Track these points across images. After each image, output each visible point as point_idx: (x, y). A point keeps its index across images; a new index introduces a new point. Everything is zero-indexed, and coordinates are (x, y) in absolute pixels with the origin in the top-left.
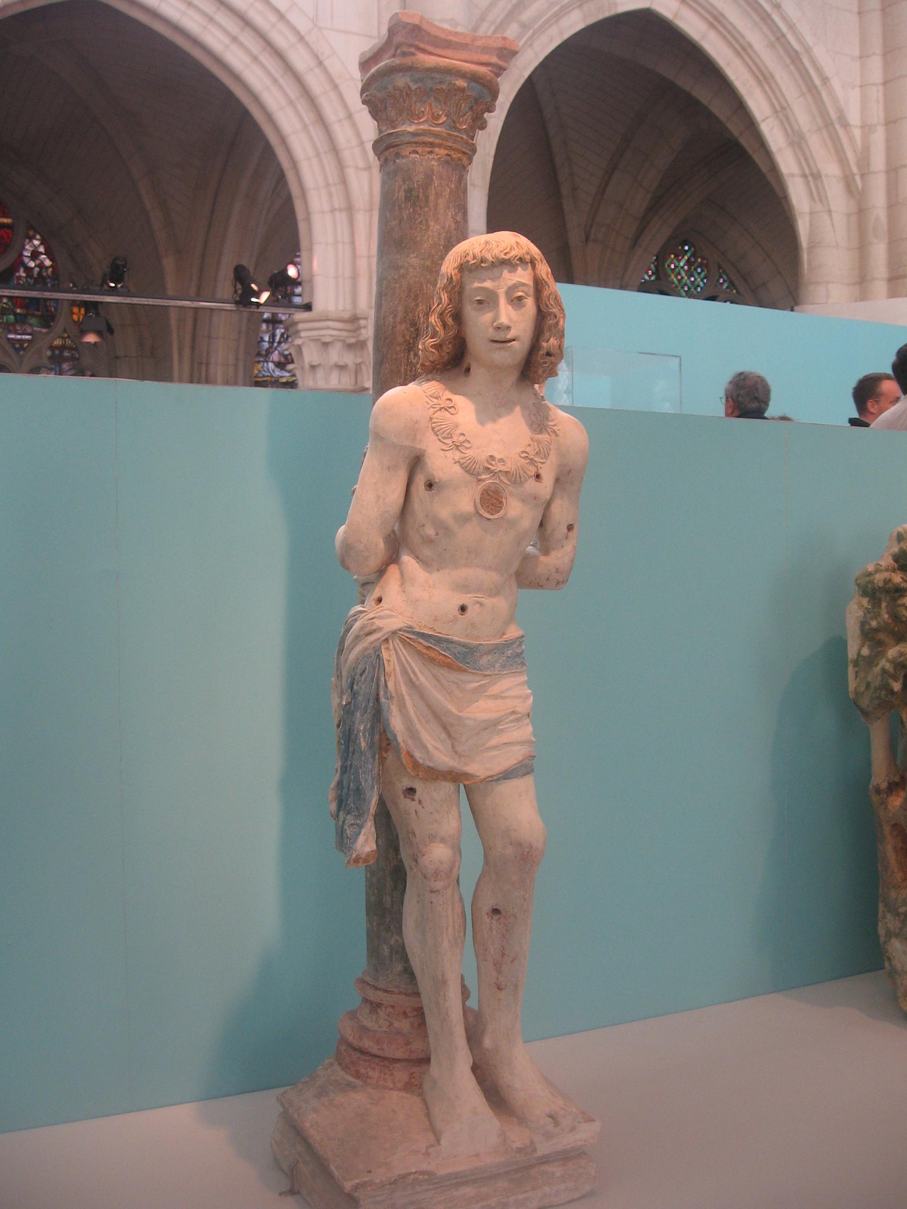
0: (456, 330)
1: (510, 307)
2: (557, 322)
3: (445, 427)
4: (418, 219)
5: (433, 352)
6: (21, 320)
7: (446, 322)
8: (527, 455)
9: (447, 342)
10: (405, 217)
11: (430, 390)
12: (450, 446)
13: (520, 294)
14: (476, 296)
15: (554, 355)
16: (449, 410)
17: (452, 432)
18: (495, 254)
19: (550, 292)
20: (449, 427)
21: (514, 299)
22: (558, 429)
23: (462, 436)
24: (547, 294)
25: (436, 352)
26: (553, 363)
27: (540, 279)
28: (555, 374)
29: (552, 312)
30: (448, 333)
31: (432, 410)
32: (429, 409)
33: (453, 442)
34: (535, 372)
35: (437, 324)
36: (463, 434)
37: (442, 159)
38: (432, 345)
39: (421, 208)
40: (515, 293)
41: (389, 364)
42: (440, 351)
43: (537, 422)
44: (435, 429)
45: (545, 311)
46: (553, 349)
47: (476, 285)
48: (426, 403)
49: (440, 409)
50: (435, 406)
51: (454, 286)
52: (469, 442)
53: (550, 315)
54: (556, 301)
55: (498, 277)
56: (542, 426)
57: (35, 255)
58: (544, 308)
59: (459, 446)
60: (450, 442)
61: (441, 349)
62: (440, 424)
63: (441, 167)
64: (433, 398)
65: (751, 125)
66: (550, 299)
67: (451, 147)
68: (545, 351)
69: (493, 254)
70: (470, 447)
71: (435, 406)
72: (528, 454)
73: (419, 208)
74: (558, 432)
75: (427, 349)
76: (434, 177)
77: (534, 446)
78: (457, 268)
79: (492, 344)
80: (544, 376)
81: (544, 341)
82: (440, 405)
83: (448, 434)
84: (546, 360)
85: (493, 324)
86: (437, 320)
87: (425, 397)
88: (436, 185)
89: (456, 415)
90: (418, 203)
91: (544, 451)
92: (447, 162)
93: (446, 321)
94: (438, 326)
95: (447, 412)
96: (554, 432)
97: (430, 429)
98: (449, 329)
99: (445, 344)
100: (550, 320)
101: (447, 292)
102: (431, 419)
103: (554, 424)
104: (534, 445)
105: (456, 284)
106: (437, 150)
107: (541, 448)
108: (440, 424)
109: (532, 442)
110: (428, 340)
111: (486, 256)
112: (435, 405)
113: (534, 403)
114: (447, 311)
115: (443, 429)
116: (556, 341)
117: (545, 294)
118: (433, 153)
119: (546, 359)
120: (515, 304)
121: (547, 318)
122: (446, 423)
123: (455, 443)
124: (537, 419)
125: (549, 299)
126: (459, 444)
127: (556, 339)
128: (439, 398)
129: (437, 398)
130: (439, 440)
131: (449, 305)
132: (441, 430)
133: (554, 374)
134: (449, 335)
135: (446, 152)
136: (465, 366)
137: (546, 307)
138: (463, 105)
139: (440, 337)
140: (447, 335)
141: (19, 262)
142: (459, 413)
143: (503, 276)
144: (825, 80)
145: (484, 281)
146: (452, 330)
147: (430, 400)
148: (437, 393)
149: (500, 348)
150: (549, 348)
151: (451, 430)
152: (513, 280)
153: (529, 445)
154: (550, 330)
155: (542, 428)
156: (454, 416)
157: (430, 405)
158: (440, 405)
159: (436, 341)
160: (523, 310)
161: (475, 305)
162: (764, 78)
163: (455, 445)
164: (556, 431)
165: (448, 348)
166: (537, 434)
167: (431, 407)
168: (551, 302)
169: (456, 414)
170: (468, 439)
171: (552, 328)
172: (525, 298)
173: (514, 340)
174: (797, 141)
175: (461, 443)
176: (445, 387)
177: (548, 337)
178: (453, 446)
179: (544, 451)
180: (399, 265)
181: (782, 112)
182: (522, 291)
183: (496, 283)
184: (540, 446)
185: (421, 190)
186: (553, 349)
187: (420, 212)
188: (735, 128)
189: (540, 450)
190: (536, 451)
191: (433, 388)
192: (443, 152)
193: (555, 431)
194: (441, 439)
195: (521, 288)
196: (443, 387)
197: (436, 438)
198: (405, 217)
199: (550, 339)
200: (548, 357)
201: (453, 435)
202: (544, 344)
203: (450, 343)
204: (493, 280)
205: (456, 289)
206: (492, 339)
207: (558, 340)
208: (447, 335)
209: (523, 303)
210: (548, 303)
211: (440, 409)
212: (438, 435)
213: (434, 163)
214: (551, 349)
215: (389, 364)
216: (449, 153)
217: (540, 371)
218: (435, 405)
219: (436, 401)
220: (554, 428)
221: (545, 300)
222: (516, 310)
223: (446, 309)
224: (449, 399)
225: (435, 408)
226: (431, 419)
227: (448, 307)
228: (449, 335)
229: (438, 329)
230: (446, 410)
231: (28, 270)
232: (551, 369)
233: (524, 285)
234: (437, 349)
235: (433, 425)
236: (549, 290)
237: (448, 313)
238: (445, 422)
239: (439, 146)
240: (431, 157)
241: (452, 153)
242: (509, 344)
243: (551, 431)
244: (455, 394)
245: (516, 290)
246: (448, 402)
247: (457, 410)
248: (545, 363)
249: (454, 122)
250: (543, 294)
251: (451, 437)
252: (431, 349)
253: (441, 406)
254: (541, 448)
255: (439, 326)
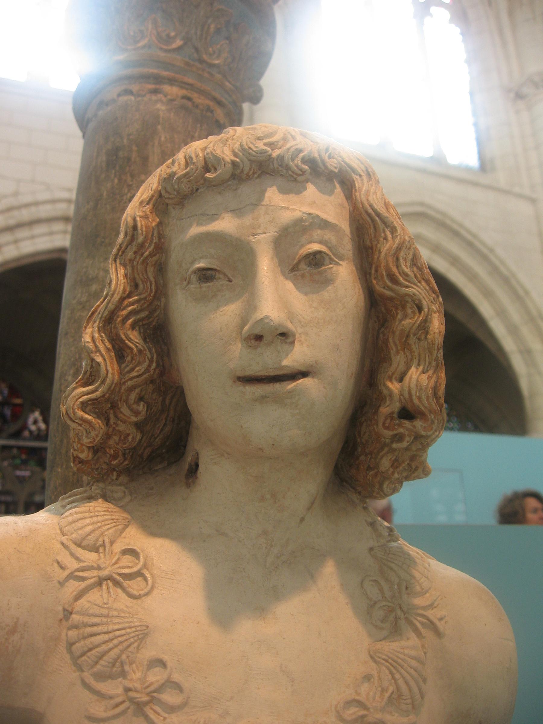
0: (151, 361)
1: (289, 285)
2: (425, 321)
3: (106, 642)
4: (126, 194)
5: (89, 423)
6: (25, 462)
7: (123, 341)
8: (363, 712)
9: (133, 396)
10: (105, 194)
11: (79, 524)
12: (117, 705)
13: (316, 247)
14: (193, 263)
15: (422, 415)
16: (125, 584)
17: (124, 657)
18: (241, 146)
19: (397, 241)
20: (116, 642)
21: (300, 261)
22: (439, 616)
23: (157, 669)
24: (391, 248)
25: (98, 423)
26: (422, 436)
27: (369, 215)
28: (424, 470)
29: (407, 295)
30: (132, 370)
31: (73, 587)
32: (61, 584)
33: (127, 690)
34: (369, 468)
35: (96, 346)
36: (162, 664)
37: (176, 103)
38: (82, 403)
39: (133, 176)
40: (302, 246)
41: (62, 467)
42: (112, 421)
43: (384, 603)
44: (74, 647)
45: (388, 293)
46: (419, 398)
47: (195, 230)
48: (56, 565)
49: (99, 583)
50: (84, 574)
51: (142, 246)
52: (178, 687)
53: (404, 307)
54: (415, 269)
55: (252, 204)
56: (399, 612)
57: (35, 422)
58: (385, 287)
59: (146, 703)
60: (120, 690)
61: (116, 416)
62: (89, 630)
63: (172, 114)
64: (84, 548)
65: (482, 323)
66: (401, 260)
67: (191, 85)
68: (396, 406)
69: (237, 146)
70: (184, 704)
71: (84, 574)
72: (366, 708)
73: (128, 175)
74: (440, 625)
75: (72, 415)
76: (159, 127)
77: (380, 679)
78: (148, 204)
79: (241, 388)
80: (396, 475)
81: (390, 379)
82: (99, 568)
83: (114, 665)
84: (401, 430)
85: (241, 332)
86: (96, 335)
87: (59, 546)
88: (163, 139)
89: (148, 601)
90: (127, 168)
91: (410, 690)
92: (183, 107)
93: (123, 337)
94: (98, 350)
95: (119, 591)
96: (432, 626)
97: (62, 648)
98: (132, 359)
99: (126, 401)
100: (405, 316)
101: (124, 265)
102: (68, 613)
103: (428, 603)
104: (379, 672)
105: (146, 237)
106: (167, 88)
107: (401, 682)
108: (89, 630)
109: (373, 664)
110: (75, 388)
111: (218, 152)
112: (83, 570)
113: (371, 549)
114: (125, 312)
115: (117, 637)
116: (424, 377)
117: (384, 251)
118: (160, 93)
119: (400, 425)
120: (303, 276)
121: (394, 317)
122: (111, 628)
123: (132, 694)
124: (382, 591)
125: (398, 260)
126: (145, 698)
127: (423, 372)
128: (101, 550)
129: (95, 549)
130: (86, 685)
131: (129, 296)
132: (90, 650)
133: (420, 470)
134: (134, 374)
135: (184, 92)
136: (189, 458)
137: (389, 283)
138: (212, 26)
139: (103, 382)
140: (127, 377)
141: (25, 427)
142: (155, 592)
143: (266, 202)
144: (527, 293)
145: (214, 217)
146: (139, 364)
147: (72, 555)
148: (98, 533)
149: (263, 399)
150: (407, 396)
151: (122, 652)
152: (294, 210)
153: (368, 678)
154: (405, 345)
155: (396, 618)
156: (139, 601)
157: (66, 573)
158: (99, 568)
159: (93, 392)
160: (327, 293)
161: (194, 286)
162: (488, 294)
163: (132, 700)
164: (437, 623)
165: (137, 413)
166: (385, 638)
167: (71, 576)
168: (403, 266)
169: (147, 594)
170: (176, 677)
171: (412, 340)
172: (332, 261)
173: (304, 374)
174: (513, 330)
175: (148, 694)
176: (125, 515)
177: (402, 367)
178: (127, 704)
179: (410, 690)
180: (90, 276)
181: (502, 313)
182: (321, 242)
183: (247, 220)
184: (397, 676)
185: (134, 148)
186: (419, 398)
187: (131, 183)
188: (472, 326)
189: (398, 689)
190: (387, 695)
191: (88, 521)
192: (174, 91)
193: (432, 623)
194: (91, 681)
195: (317, 233)
196: (119, 515)
197: (74, 675)
198: (105, 194)
199: (408, 368)
200: (407, 423)
201: (127, 668)
202: (394, 387)
203: (141, 399)
204: (238, 212)
205: (147, 253)
206: (240, 374)
207: (430, 372)
208: (127, 377)
209: (326, 271)
210: (395, 270)
211: (99, 583)
212: (80, 668)
213: (159, 106)
214: (416, 401)
215: (62, 467)
216: (189, 95)
217: (385, 463)
218: (83, 570)
219: (90, 557)
220: (430, 613)
221: (387, 266)
222: (306, 294)
223: (119, 306)
224: (132, 552)
225: (83, 579)
226: (68, 613)
227: (126, 302)
228: (134, 374)
229: (99, 359)
230: (117, 584)
231: (31, 432)
232: (413, 458)
233: (325, 224)
234: (101, 414)
235: (71, 633)
236: (393, 238)
237: (127, 317)
238: (107, 623)
239: (171, 81)
240: (154, 98)
241: (195, 96)
242: (291, 386)
243: (422, 624)
244: (153, 534)
245: (303, 240)
246: (127, 560)
247: (150, 583)
248: (399, 438)
249: (197, 50)
250: (380, 252)
251: (123, 674)
252: (80, 413)
253: (105, 573)
254: (401, 682)
255: (104, 353)
